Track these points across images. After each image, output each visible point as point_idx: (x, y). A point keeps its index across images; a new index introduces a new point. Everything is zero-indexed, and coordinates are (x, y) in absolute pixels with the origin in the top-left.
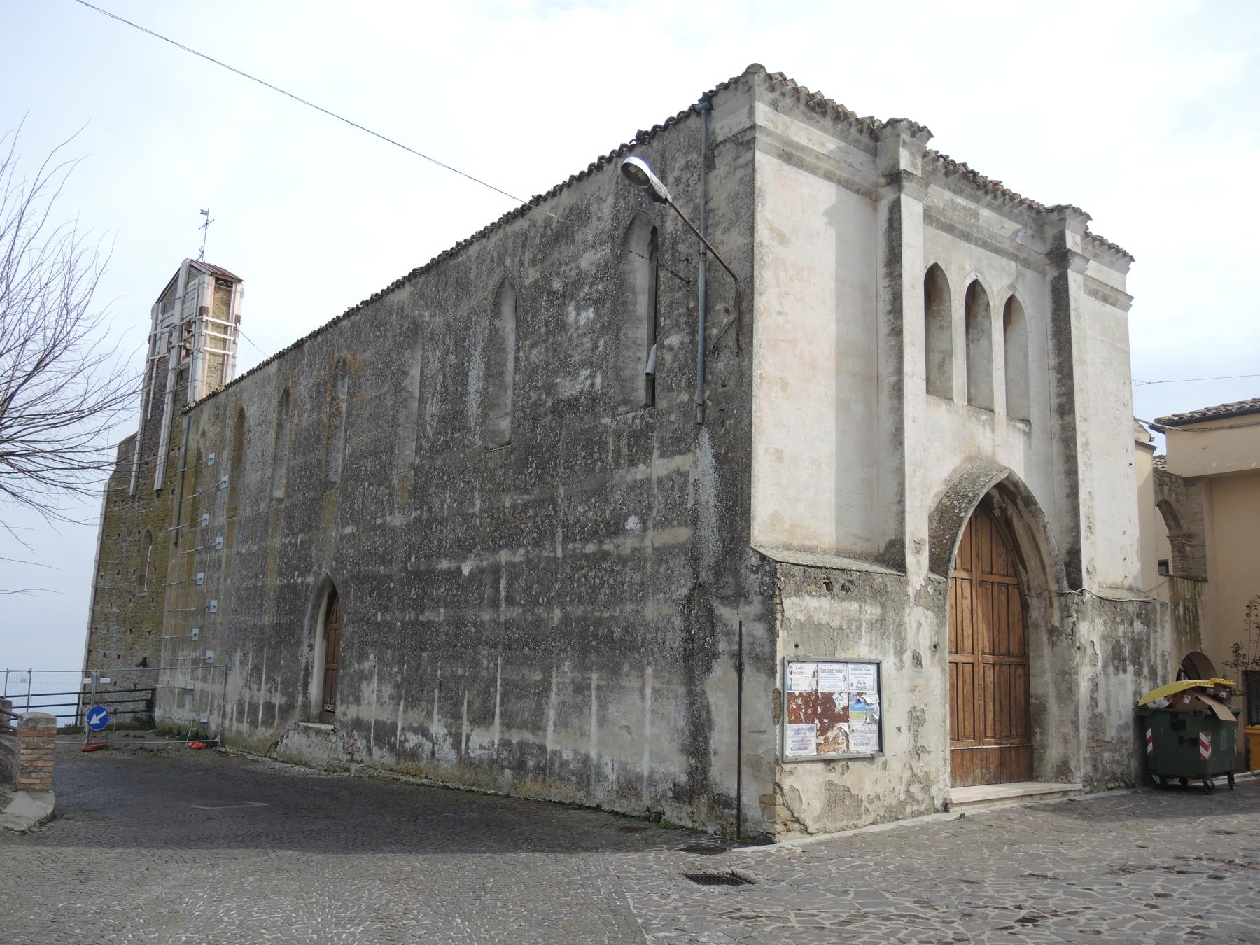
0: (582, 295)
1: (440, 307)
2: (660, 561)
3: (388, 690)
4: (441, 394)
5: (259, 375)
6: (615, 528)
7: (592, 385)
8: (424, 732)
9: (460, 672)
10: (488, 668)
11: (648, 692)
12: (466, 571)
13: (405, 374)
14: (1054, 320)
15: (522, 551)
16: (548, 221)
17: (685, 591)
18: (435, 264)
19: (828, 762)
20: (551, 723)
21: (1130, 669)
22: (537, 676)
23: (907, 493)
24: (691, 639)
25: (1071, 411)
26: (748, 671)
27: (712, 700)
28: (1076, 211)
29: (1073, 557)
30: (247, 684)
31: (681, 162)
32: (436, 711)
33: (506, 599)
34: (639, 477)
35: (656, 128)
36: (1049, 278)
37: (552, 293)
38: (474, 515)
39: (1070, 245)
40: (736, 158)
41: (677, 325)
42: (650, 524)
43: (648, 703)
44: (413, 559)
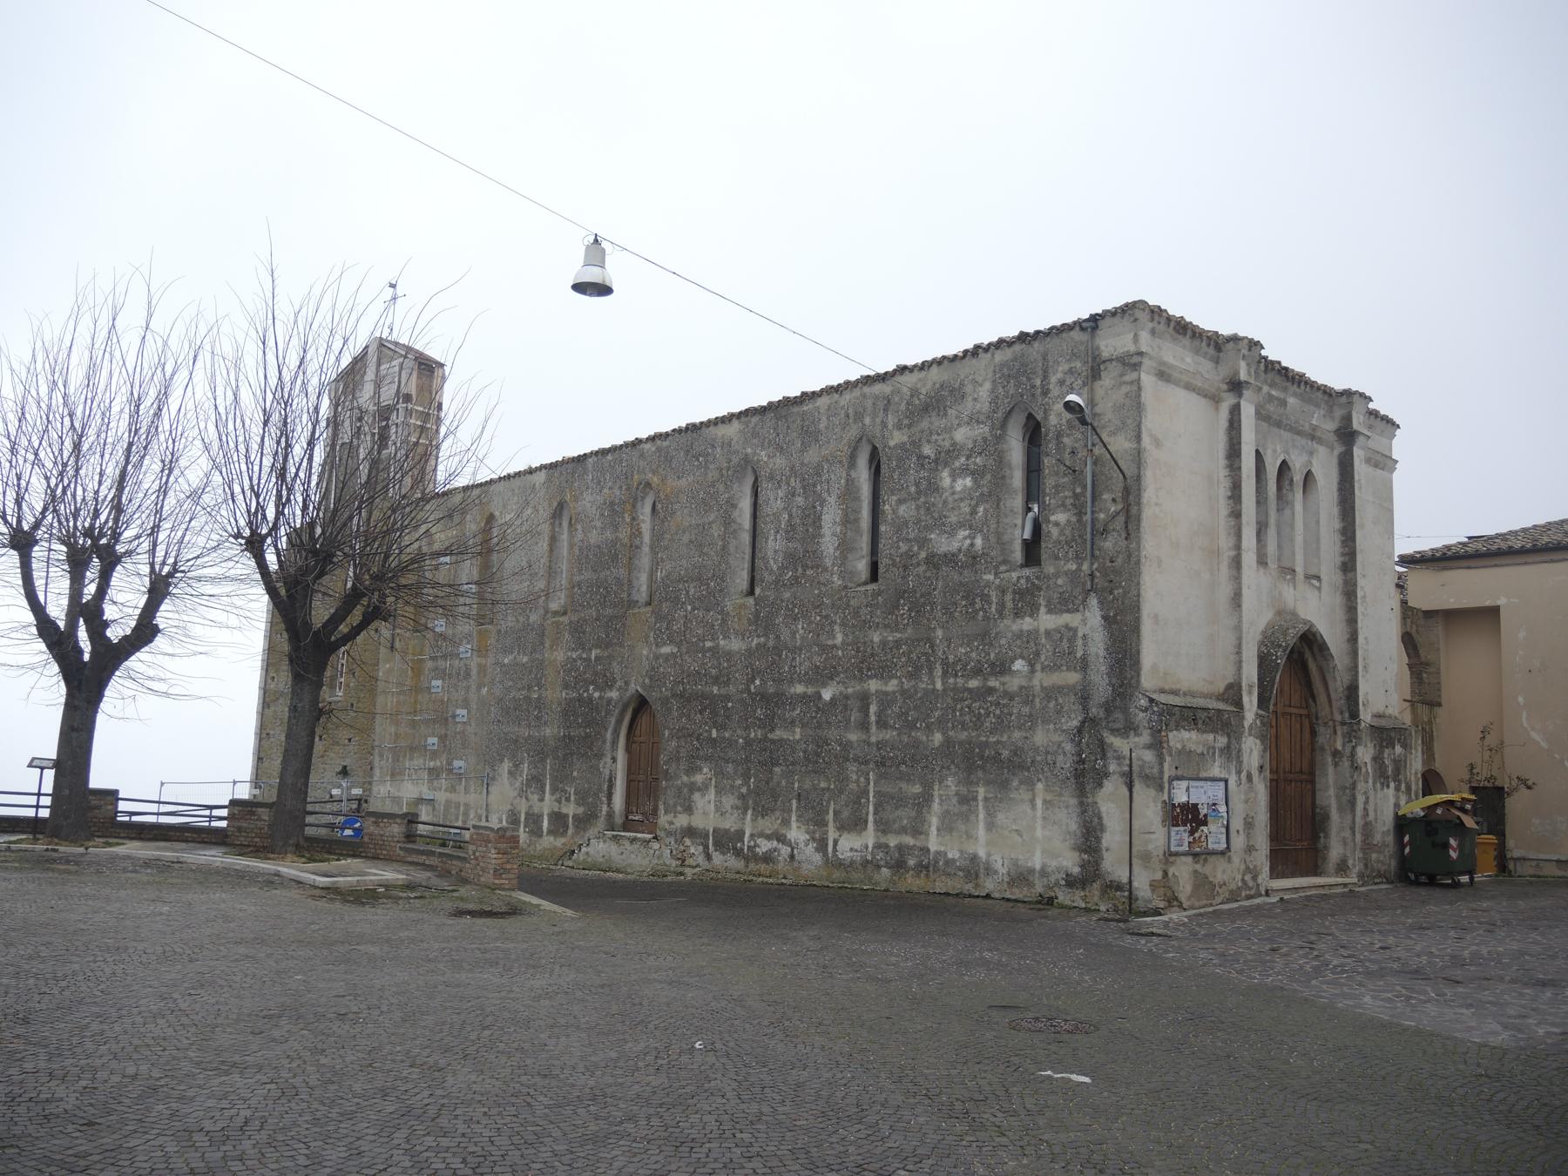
0: (957, 464)
1: (780, 449)
2: (1048, 698)
3: (729, 801)
4: (787, 532)
5: (517, 482)
6: (1001, 668)
7: (972, 545)
8: (781, 839)
9: (823, 785)
10: (857, 781)
11: (1039, 803)
12: (827, 695)
13: (734, 506)
14: (1340, 489)
15: (895, 682)
16: (915, 392)
17: (1075, 723)
18: (771, 407)
19: (1195, 855)
20: (933, 830)
21: (1392, 785)
22: (917, 789)
23: (1244, 647)
24: (1083, 762)
25: (1354, 569)
26: (1137, 787)
27: (1103, 809)
28: (1362, 395)
29: (1352, 691)
30: (522, 793)
31: (1066, 367)
32: (794, 818)
33: (877, 722)
34: (1025, 627)
35: (1037, 332)
36: (1336, 452)
37: (921, 457)
38: (834, 646)
39: (1356, 425)
40: (1122, 375)
41: (1063, 505)
42: (1038, 667)
43: (1039, 813)
44: (758, 682)
